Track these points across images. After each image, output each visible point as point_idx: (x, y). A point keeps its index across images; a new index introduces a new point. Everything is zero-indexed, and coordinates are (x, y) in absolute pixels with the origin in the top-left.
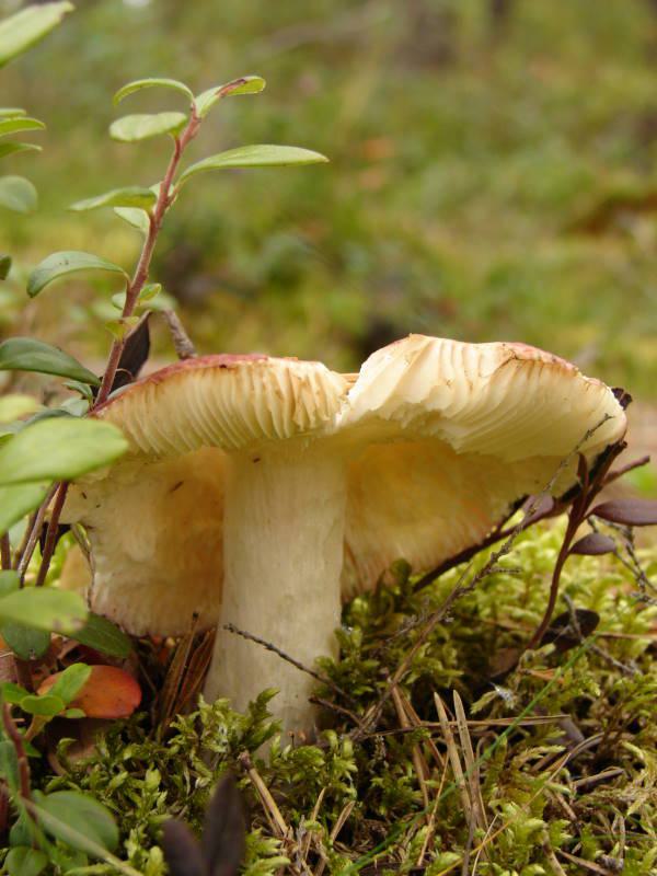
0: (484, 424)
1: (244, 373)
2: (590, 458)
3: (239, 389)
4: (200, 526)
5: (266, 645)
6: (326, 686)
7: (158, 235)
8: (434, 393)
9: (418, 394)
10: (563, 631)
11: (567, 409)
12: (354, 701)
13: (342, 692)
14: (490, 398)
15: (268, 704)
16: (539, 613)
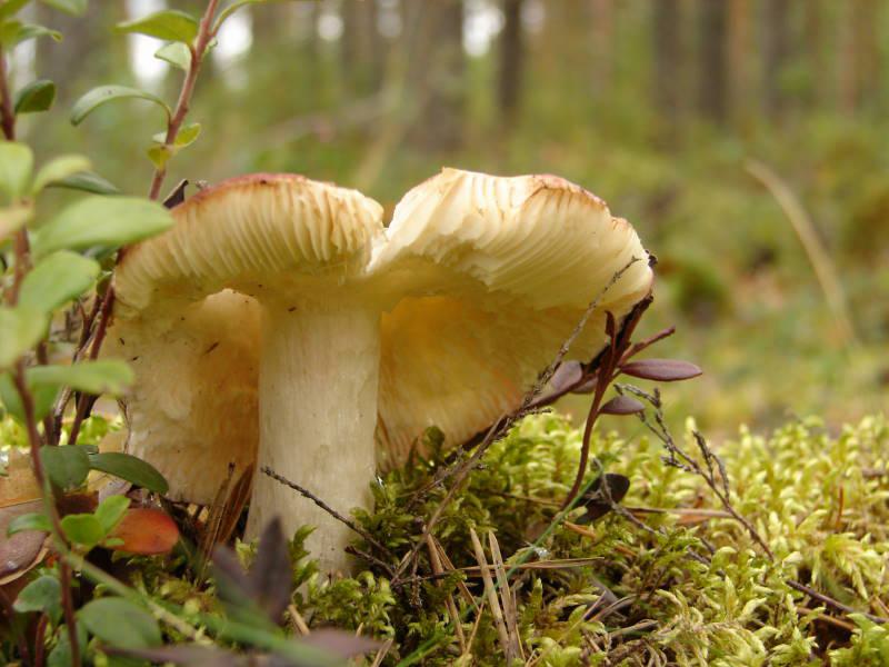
0: (514, 256)
1: (283, 190)
2: (618, 316)
3: (279, 206)
4: (235, 390)
5: (302, 491)
6: (361, 538)
7: (199, 69)
8: (468, 223)
9: (451, 226)
10: (594, 496)
11: (596, 245)
12: (388, 553)
13: (377, 544)
14: (521, 226)
15: (305, 541)
16: (569, 486)
